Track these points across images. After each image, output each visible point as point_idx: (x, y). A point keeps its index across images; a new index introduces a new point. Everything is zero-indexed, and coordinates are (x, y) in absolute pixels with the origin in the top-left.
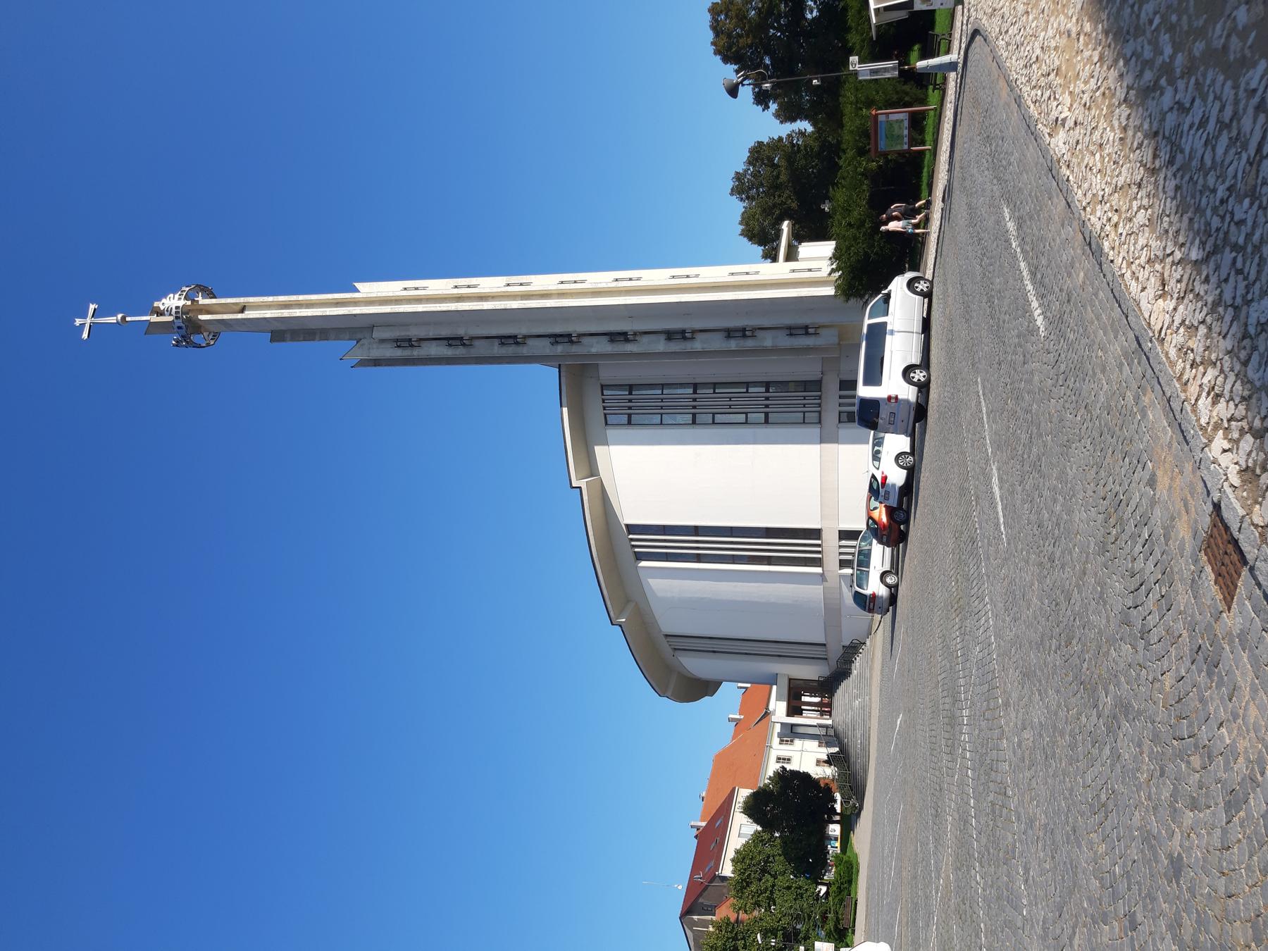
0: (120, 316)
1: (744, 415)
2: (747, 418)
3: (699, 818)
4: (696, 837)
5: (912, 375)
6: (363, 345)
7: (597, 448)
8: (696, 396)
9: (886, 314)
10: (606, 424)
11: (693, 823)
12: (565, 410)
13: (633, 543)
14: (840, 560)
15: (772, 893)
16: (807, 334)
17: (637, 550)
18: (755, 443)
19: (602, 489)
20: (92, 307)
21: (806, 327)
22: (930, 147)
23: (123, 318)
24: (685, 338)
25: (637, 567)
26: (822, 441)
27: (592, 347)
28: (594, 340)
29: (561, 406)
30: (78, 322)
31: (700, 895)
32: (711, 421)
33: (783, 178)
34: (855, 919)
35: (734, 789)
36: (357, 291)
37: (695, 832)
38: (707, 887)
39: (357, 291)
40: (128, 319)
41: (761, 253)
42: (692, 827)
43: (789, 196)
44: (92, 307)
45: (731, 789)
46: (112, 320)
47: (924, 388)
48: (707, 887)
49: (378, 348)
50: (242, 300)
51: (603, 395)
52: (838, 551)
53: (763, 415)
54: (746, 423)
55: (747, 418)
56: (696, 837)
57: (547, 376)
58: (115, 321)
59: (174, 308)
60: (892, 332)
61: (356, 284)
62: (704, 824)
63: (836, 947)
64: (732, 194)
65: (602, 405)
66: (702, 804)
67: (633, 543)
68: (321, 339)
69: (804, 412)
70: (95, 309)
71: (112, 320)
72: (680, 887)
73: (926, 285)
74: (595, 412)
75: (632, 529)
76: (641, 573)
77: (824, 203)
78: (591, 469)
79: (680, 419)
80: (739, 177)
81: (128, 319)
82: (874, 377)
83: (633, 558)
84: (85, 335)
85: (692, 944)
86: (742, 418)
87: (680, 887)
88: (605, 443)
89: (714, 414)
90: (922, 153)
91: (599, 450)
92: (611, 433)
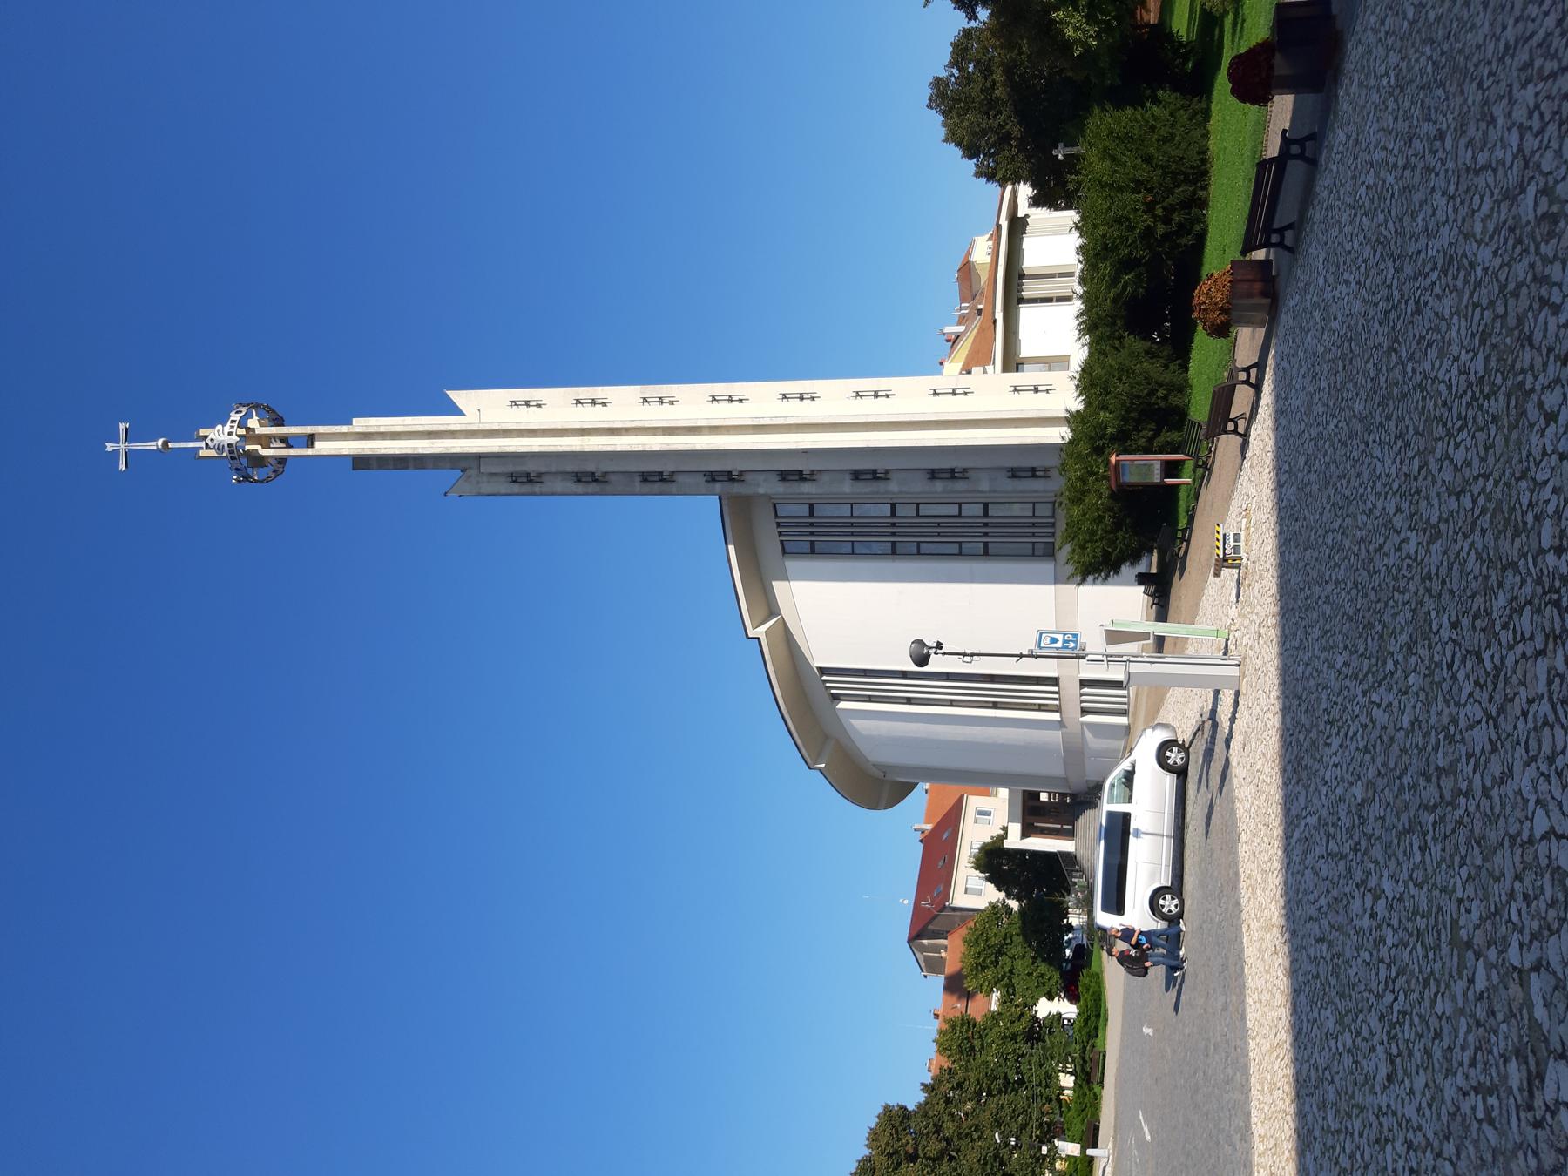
0: (160, 442)
1: (957, 506)
2: (960, 548)
3: (923, 817)
4: (921, 841)
5: (1168, 754)
6: (470, 477)
7: (775, 584)
8: (895, 520)
9: (1130, 800)
10: (784, 552)
11: (916, 826)
12: (731, 548)
13: (828, 685)
14: (1082, 708)
15: (1010, 979)
16: (1034, 476)
17: (833, 691)
18: (972, 581)
19: (787, 637)
20: (122, 426)
21: (1033, 470)
22: (1189, 480)
23: (165, 444)
24: (876, 478)
25: (835, 709)
26: (1056, 581)
27: (758, 485)
28: (761, 477)
29: (726, 543)
30: (110, 447)
31: (930, 922)
32: (915, 551)
33: (999, 92)
34: (1103, 1074)
35: (962, 797)
36: (457, 411)
37: (919, 836)
38: (936, 916)
39: (457, 411)
40: (170, 445)
41: (973, 169)
42: (915, 830)
43: (1010, 117)
44: (122, 426)
45: (958, 797)
46: (151, 446)
47: (1174, 920)
48: (936, 916)
49: (488, 482)
50: (309, 430)
51: (776, 516)
52: (1078, 699)
53: (981, 545)
54: (960, 554)
55: (960, 548)
56: (921, 841)
57: (707, 507)
58: (155, 448)
59: (226, 446)
60: (1137, 833)
61: (451, 394)
62: (929, 827)
63: (1082, 1147)
64: (929, 106)
65: (775, 531)
66: (926, 797)
67: (828, 685)
68: (416, 468)
69: (1034, 516)
70: (127, 429)
71: (151, 446)
72: (906, 902)
73: (1172, 908)
74: (769, 541)
75: (823, 671)
76: (841, 715)
77: (1057, 148)
78: (771, 609)
79: (876, 548)
80: (938, 83)
81: (170, 445)
82: (1116, 903)
83: (828, 699)
84: (122, 467)
85: (923, 965)
86: (954, 549)
87: (906, 902)
88: (785, 577)
89: (959, 516)
90: (1176, 487)
91: (778, 586)
92: (791, 565)
